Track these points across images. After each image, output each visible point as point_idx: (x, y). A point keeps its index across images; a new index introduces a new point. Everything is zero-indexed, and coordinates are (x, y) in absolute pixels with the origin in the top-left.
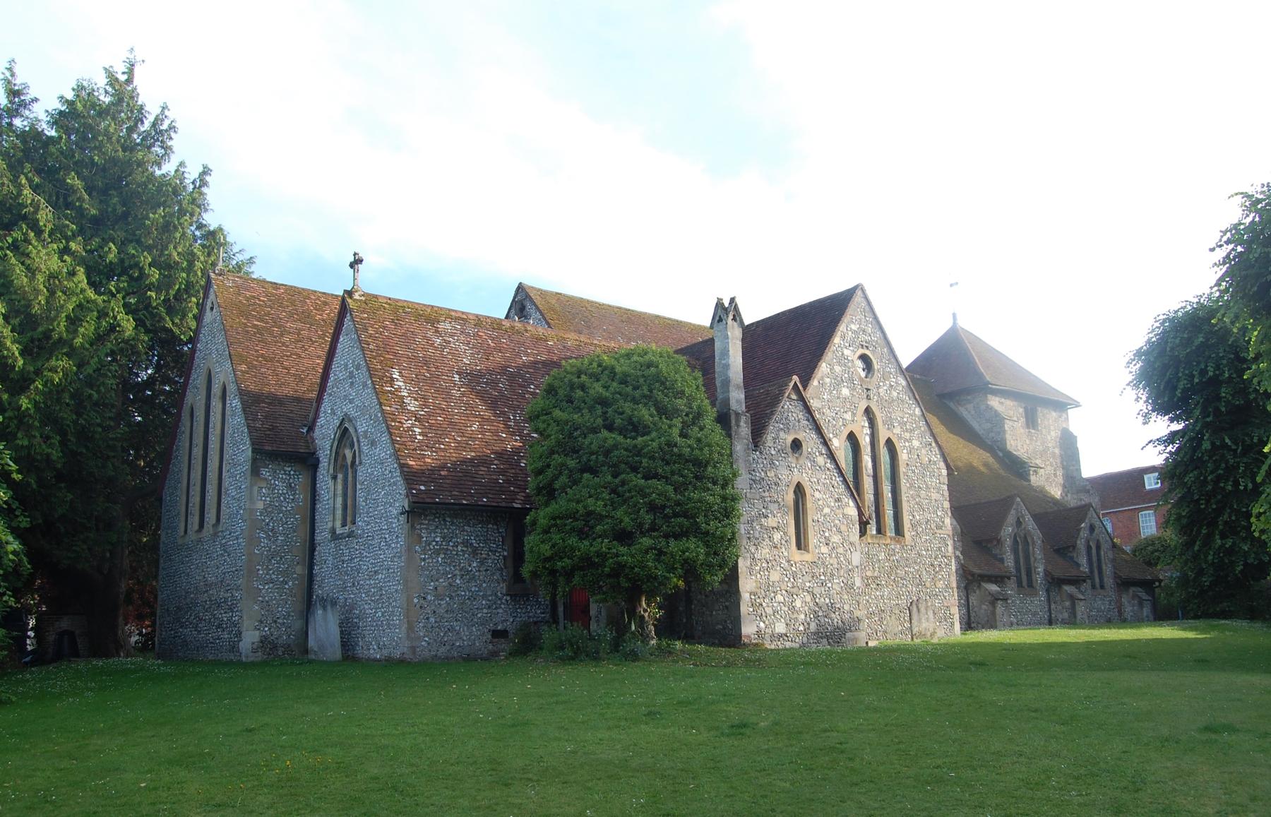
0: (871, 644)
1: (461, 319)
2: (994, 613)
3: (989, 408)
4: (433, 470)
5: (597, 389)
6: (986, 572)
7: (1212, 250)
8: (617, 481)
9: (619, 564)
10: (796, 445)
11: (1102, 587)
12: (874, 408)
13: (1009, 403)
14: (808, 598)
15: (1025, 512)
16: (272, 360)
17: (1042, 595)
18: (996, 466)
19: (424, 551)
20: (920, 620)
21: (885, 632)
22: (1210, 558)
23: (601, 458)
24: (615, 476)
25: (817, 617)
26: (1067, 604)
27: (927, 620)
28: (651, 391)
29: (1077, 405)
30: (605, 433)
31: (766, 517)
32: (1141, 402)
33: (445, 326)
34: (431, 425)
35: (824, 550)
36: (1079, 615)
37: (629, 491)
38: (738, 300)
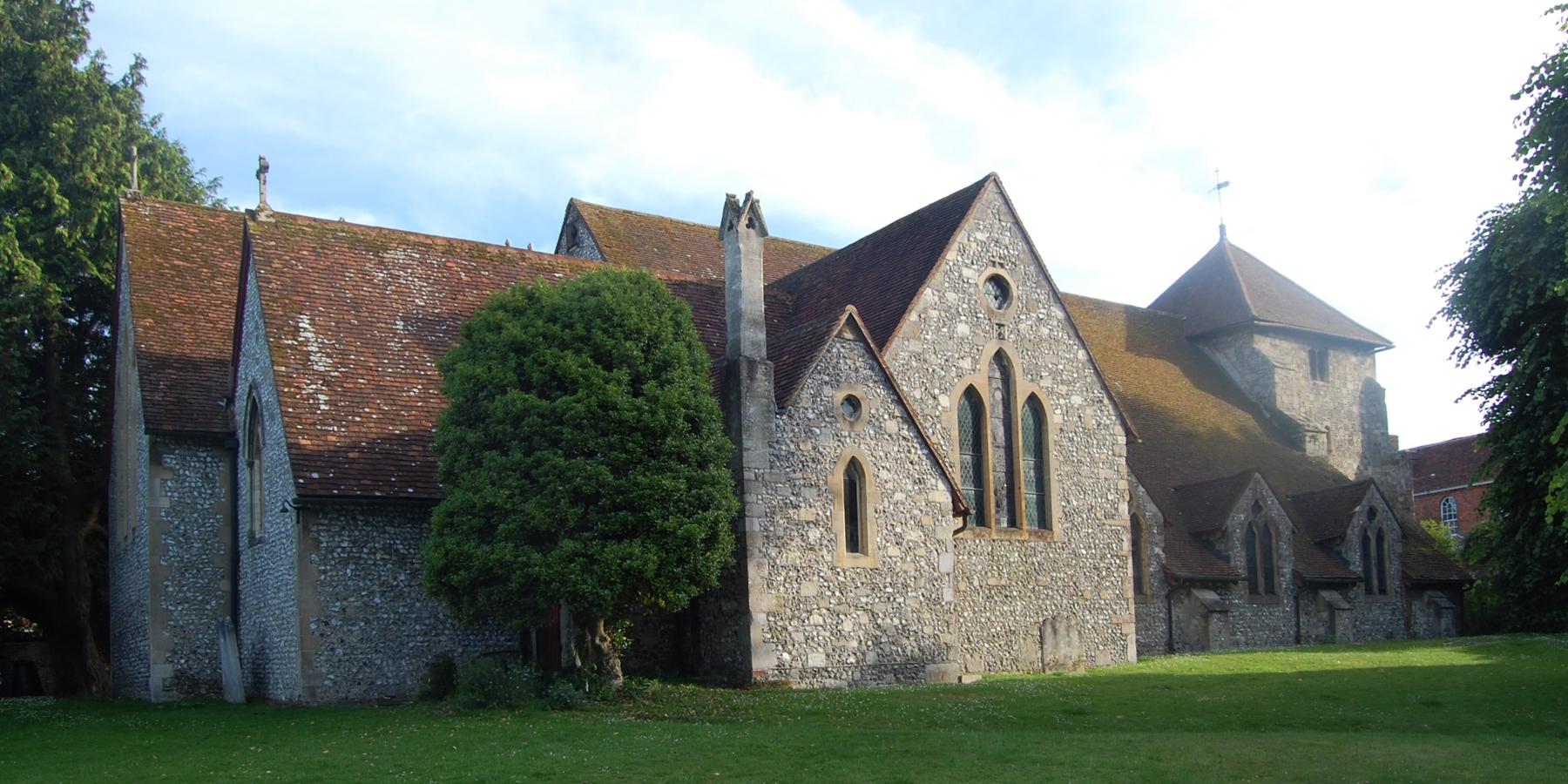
0: (967, 680)
1: (424, 245)
2: (1206, 630)
3: (1255, 353)
4: (337, 451)
5: (513, 330)
6: (1197, 576)
7: (1516, 97)
8: (530, 460)
9: (529, 576)
10: (853, 402)
11: (1383, 591)
12: (1010, 352)
13: (1286, 345)
14: (864, 619)
15: (1267, 492)
16: (191, 312)
17: (1288, 605)
18: (1258, 431)
19: (324, 561)
20: (1056, 645)
21: (1015, 660)
22: (1536, 550)
23: (510, 429)
24: (527, 454)
25: (877, 642)
26: (1325, 615)
27: (1069, 644)
28: (589, 331)
29: (1388, 345)
30: (514, 394)
31: (797, 507)
32: (1458, 337)
33: (397, 255)
34: (346, 390)
35: (894, 551)
36: (1340, 630)
37: (546, 475)
38: (755, 196)
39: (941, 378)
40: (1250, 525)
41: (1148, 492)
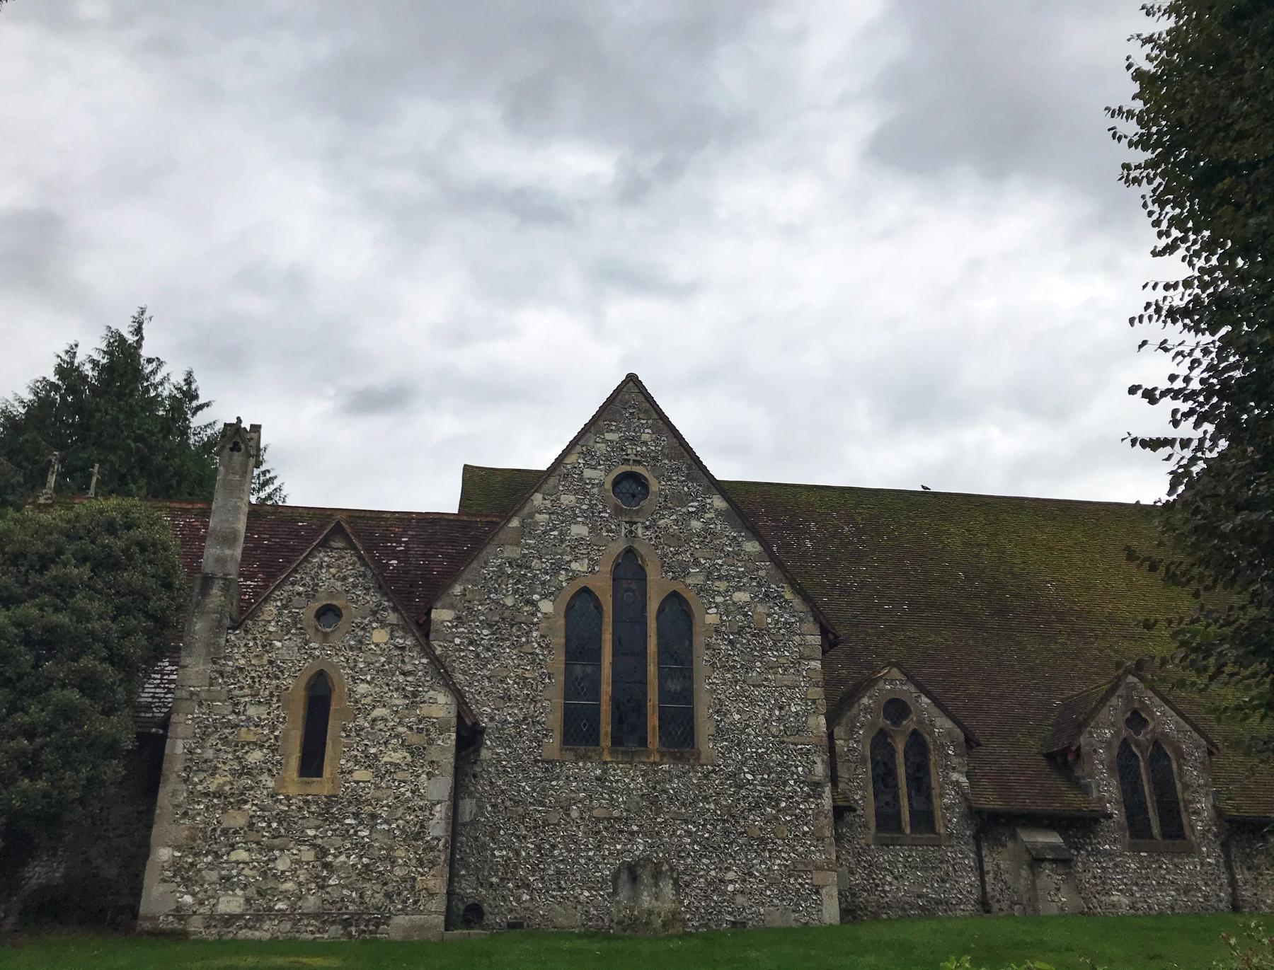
14: (308, 855)
39: (543, 583)
40: (1125, 743)
41: (936, 702)
